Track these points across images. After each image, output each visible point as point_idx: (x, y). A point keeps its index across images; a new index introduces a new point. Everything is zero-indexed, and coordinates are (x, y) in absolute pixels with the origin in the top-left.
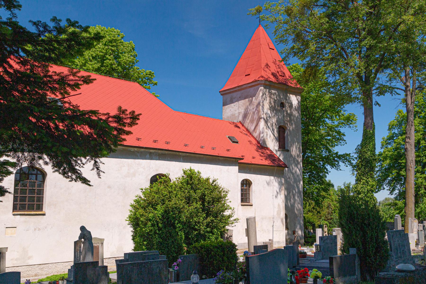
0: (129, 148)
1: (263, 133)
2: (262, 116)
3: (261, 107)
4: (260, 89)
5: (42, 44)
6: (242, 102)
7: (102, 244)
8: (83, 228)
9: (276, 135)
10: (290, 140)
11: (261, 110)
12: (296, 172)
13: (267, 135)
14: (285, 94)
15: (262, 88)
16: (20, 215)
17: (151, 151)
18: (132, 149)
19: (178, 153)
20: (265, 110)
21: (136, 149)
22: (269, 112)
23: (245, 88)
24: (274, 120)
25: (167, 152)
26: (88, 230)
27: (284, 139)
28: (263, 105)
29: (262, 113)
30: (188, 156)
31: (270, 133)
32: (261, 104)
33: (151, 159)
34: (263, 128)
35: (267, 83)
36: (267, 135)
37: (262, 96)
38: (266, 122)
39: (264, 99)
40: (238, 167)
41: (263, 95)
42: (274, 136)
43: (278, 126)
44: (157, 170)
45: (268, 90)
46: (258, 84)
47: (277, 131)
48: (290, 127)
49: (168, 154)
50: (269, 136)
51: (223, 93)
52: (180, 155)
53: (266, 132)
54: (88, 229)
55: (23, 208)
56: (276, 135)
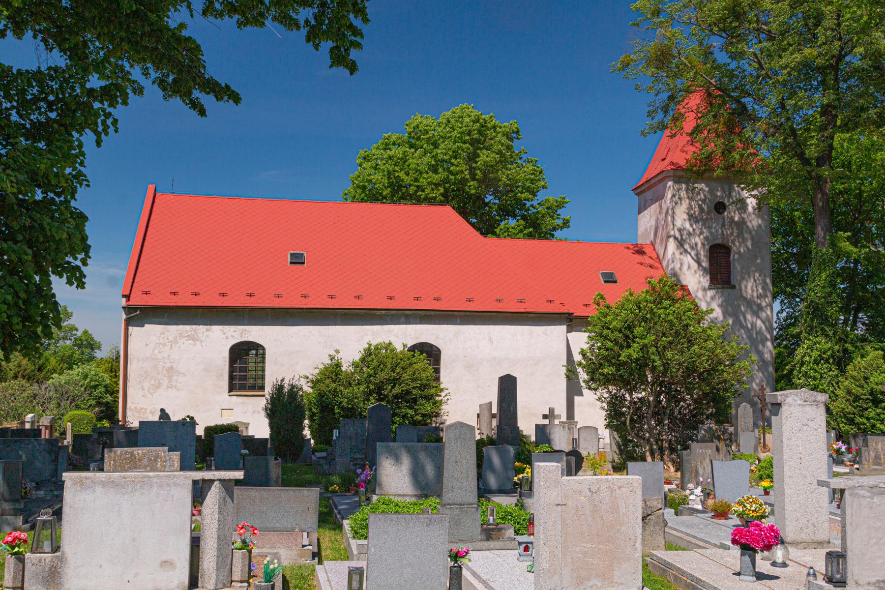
0: (373, 311)
1: (673, 262)
2: (672, 233)
3: (669, 218)
4: (668, 185)
5: (674, 5)
6: (653, 206)
7: (247, 428)
8: (162, 410)
9: (704, 264)
10: (739, 269)
11: (670, 223)
12: (754, 325)
13: (681, 264)
14: (726, 187)
15: (670, 183)
16: (237, 395)
17: (407, 312)
18: (378, 313)
19: (451, 313)
20: (679, 223)
21: (383, 312)
22: (687, 225)
23: (655, 184)
24: (698, 240)
25: (432, 313)
26: (519, 425)
27: (729, 266)
28: (674, 213)
29: (672, 226)
30: (469, 315)
31: (688, 260)
32: (670, 212)
33: (409, 323)
34: (674, 254)
35: (680, 173)
36: (681, 264)
37: (672, 198)
38: (681, 243)
39: (676, 204)
40: (565, 327)
41: (674, 196)
42: (699, 264)
43: (707, 247)
44: (417, 338)
45: (684, 186)
46: (665, 178)
47: (705, 256)
48: (739, 248)
49: (435, 316)
50: (685, 267)
51: (639, 190)
52: (456, 316)
53: (680, 259)
54: (167, 411)
55: (243, 388)
56: (705, 264)
